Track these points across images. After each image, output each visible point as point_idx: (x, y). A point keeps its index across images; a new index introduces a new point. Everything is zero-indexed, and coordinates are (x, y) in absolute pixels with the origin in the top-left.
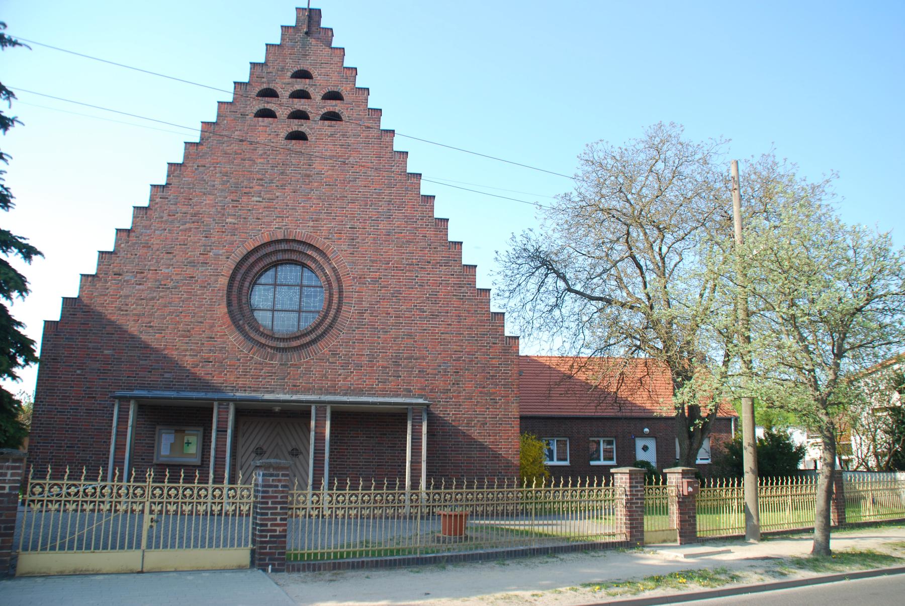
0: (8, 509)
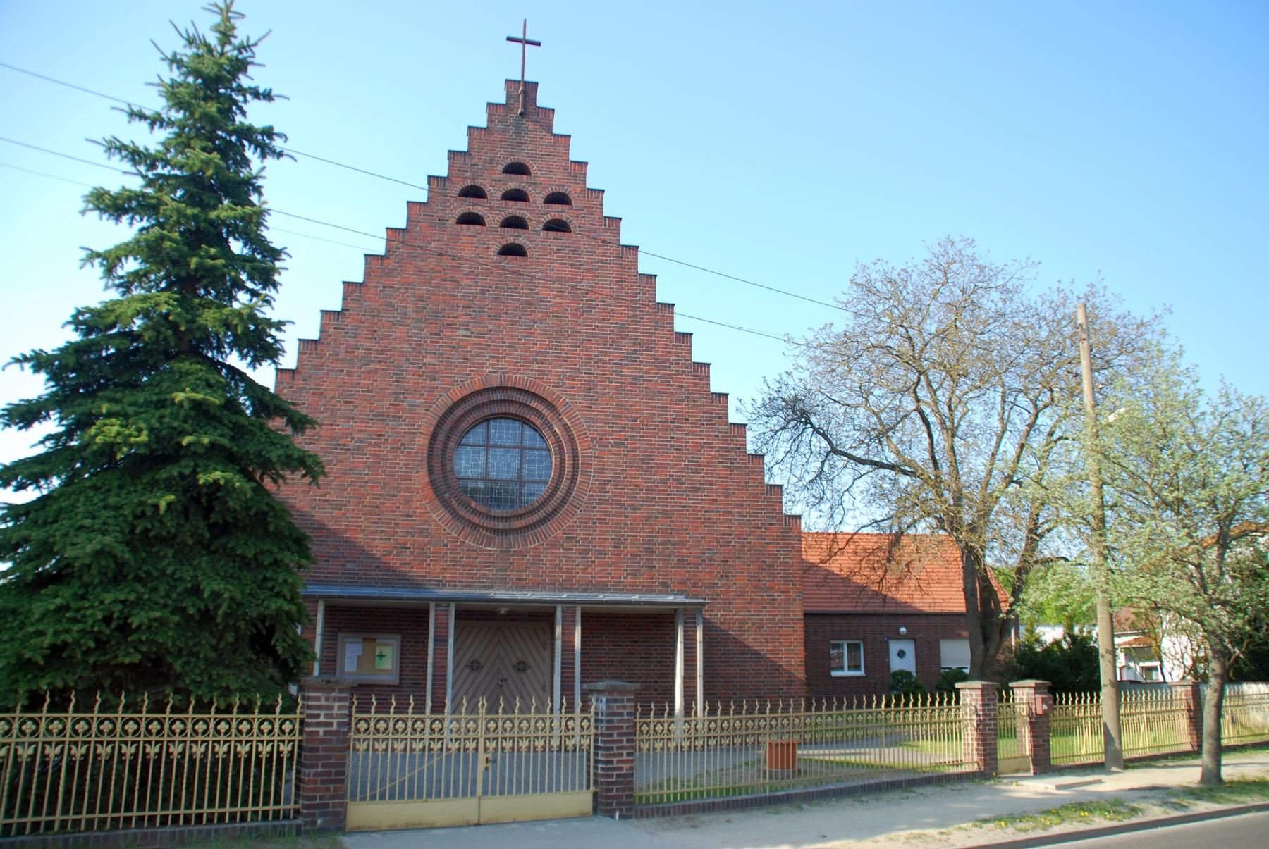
0: (338, 749)
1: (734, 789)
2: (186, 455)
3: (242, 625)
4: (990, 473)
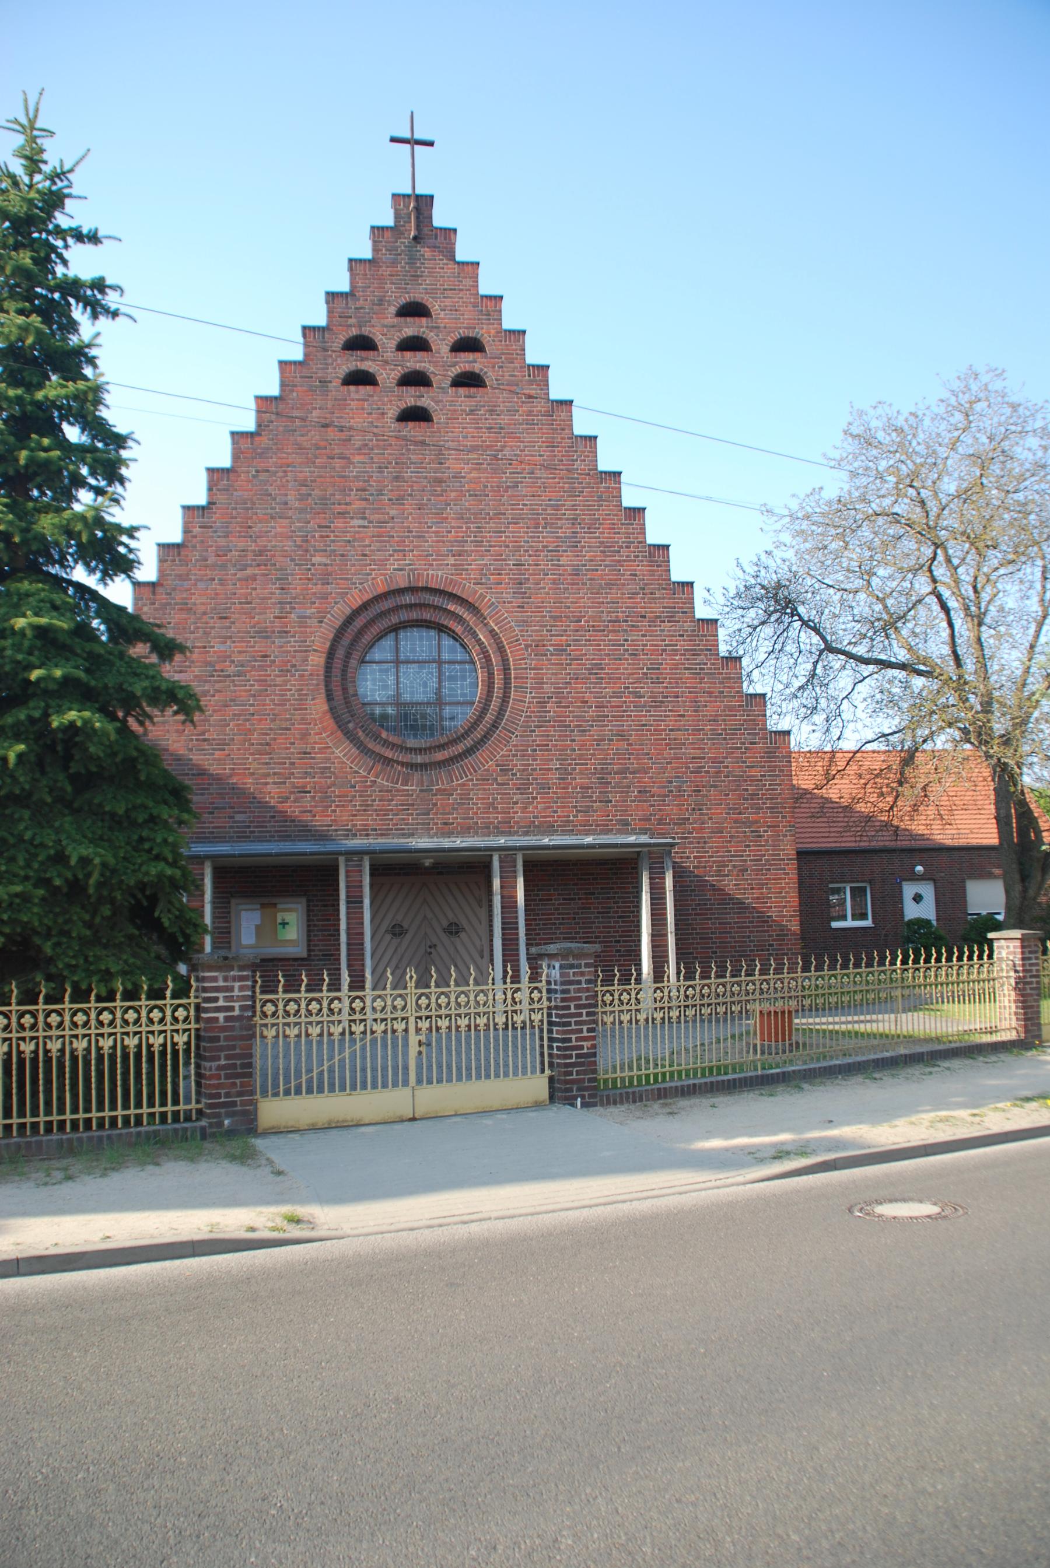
0: (242, 1038)
1: (719, 1068)
2: (34, 695)
3: (118, 895)
4: (1027, 670)
